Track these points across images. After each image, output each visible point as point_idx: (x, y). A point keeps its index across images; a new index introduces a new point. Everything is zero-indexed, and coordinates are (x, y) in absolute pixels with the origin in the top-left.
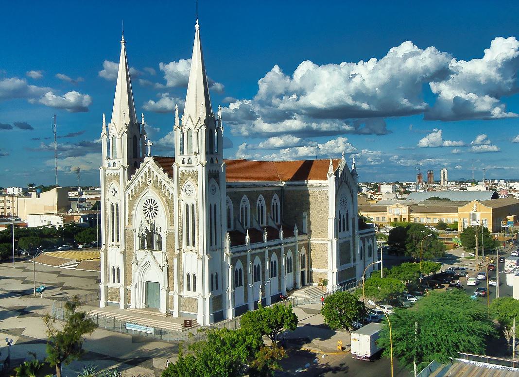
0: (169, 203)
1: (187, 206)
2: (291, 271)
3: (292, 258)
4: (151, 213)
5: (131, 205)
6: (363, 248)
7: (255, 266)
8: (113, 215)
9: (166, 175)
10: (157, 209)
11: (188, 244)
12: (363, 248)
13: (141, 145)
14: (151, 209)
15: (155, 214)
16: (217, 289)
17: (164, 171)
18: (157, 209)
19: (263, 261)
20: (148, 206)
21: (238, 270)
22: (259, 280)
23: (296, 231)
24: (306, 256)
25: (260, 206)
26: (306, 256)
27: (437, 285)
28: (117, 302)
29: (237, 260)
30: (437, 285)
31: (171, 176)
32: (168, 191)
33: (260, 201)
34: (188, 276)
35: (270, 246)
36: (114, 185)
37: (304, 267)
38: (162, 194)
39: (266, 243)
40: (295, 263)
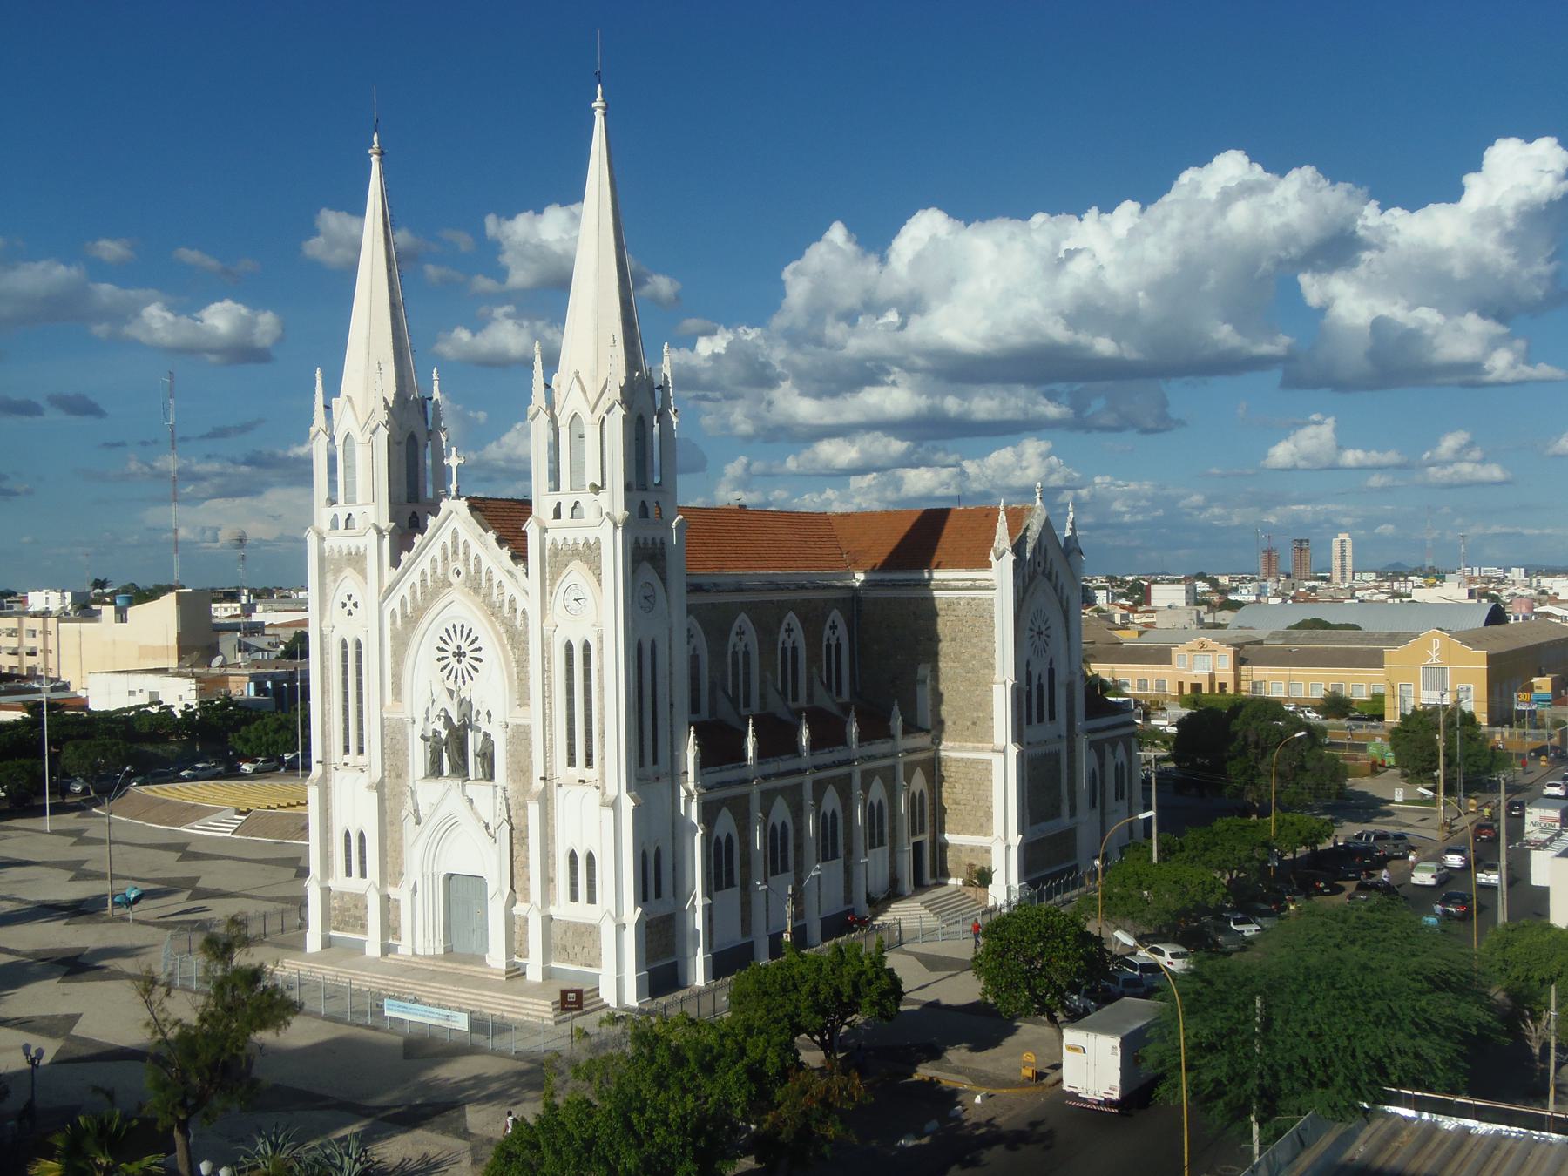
0: (516, 639)
1: (344, 645)
5: (401, 642)
6: (1098, 773)
9: (506, 553)
14: (459, 654)
20: (452, 648)
23: (897, 723)
25: (789, 646)
31: (520, 556)
34: (573, 856)
35: (818, 768)
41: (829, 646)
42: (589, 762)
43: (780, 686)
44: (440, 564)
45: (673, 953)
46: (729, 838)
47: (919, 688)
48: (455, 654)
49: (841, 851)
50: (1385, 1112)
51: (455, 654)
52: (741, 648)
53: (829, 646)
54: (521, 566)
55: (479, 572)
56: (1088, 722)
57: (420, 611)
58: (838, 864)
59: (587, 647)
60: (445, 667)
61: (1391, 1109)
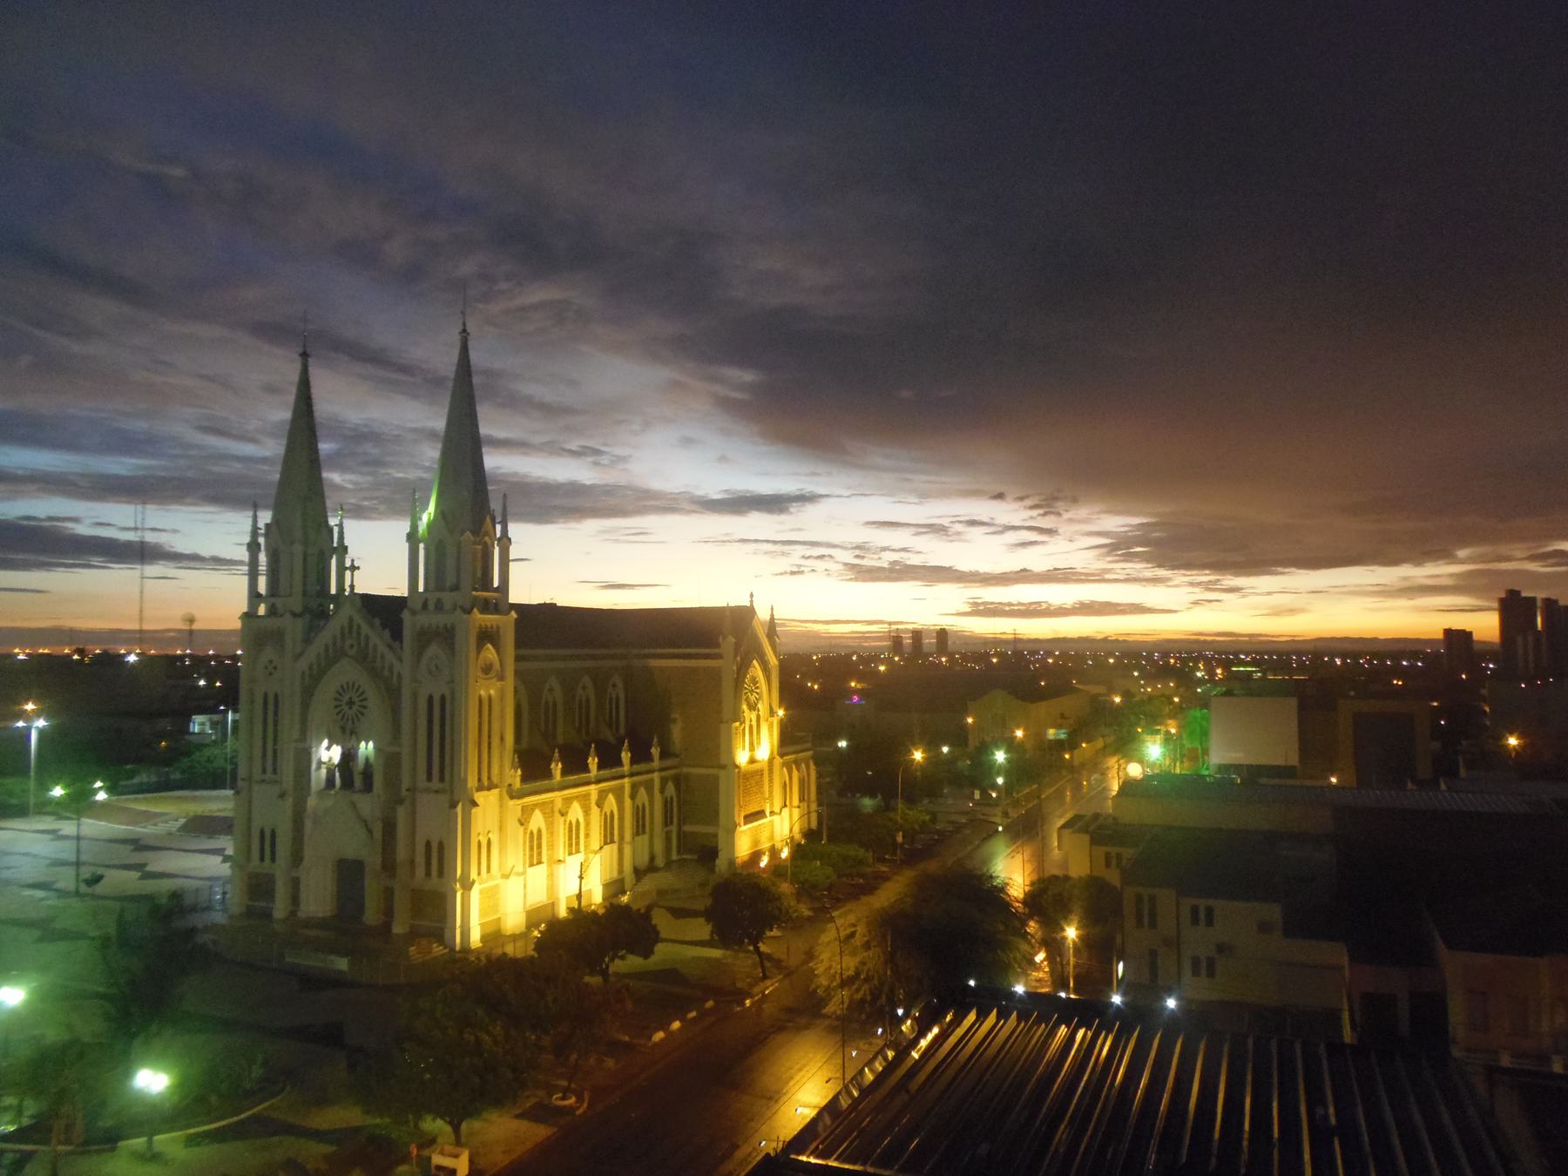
0: (392, 694)
1: (430, 699)
2: (644, 832)
3: (647, 804)
4: (350, 712)
5: (308, 693)
6: (806, 778)
7: (571, 823)
8: (265, 713)
9: (387, 634)
10: (364, 703)
11: (429, 778)
12: (806, 778)
13: (21, 557)
14: (351, 703)
15: (360, 716)
16: (489, 870)
17: (384, 626)
18: (364, 703)
19: (587, 812)
20: (346, 699)
21: (669, 799)
22: (644, 832)
23: (655, 751)
24: (675, 799)
25: (614, 696)
26: (675, 799)
27: (751, 930)
28: (263, 904)
29: (533, 810)
30: (755, 932)
31: (397, 635)
32: (391, 668)
33: (584, 688)
34: (428, 845)
35: (648, 772)
36: (490, 652)
37: (672, 823)
38: (374, 673)
39: (626, 768)
40: (652, 814)
41: (611, 699)
42: (442, 779)
43: (577, 725)
44: (339, 640)
45: (497, 911)
46: (539, 831)
47: (672, 726)
48: (354, 703)
49: (616, 838)
50: (1115, 539)
51: (354, 703)
52: (551, 700)
53: (611, 699)
54: (397, 643)
55: (367, 645)
56: (601, 772)
57: (323, 671)
58: (646, 837)
59: (276, 696)
60: (340, 712)
61: (1112, 541)
